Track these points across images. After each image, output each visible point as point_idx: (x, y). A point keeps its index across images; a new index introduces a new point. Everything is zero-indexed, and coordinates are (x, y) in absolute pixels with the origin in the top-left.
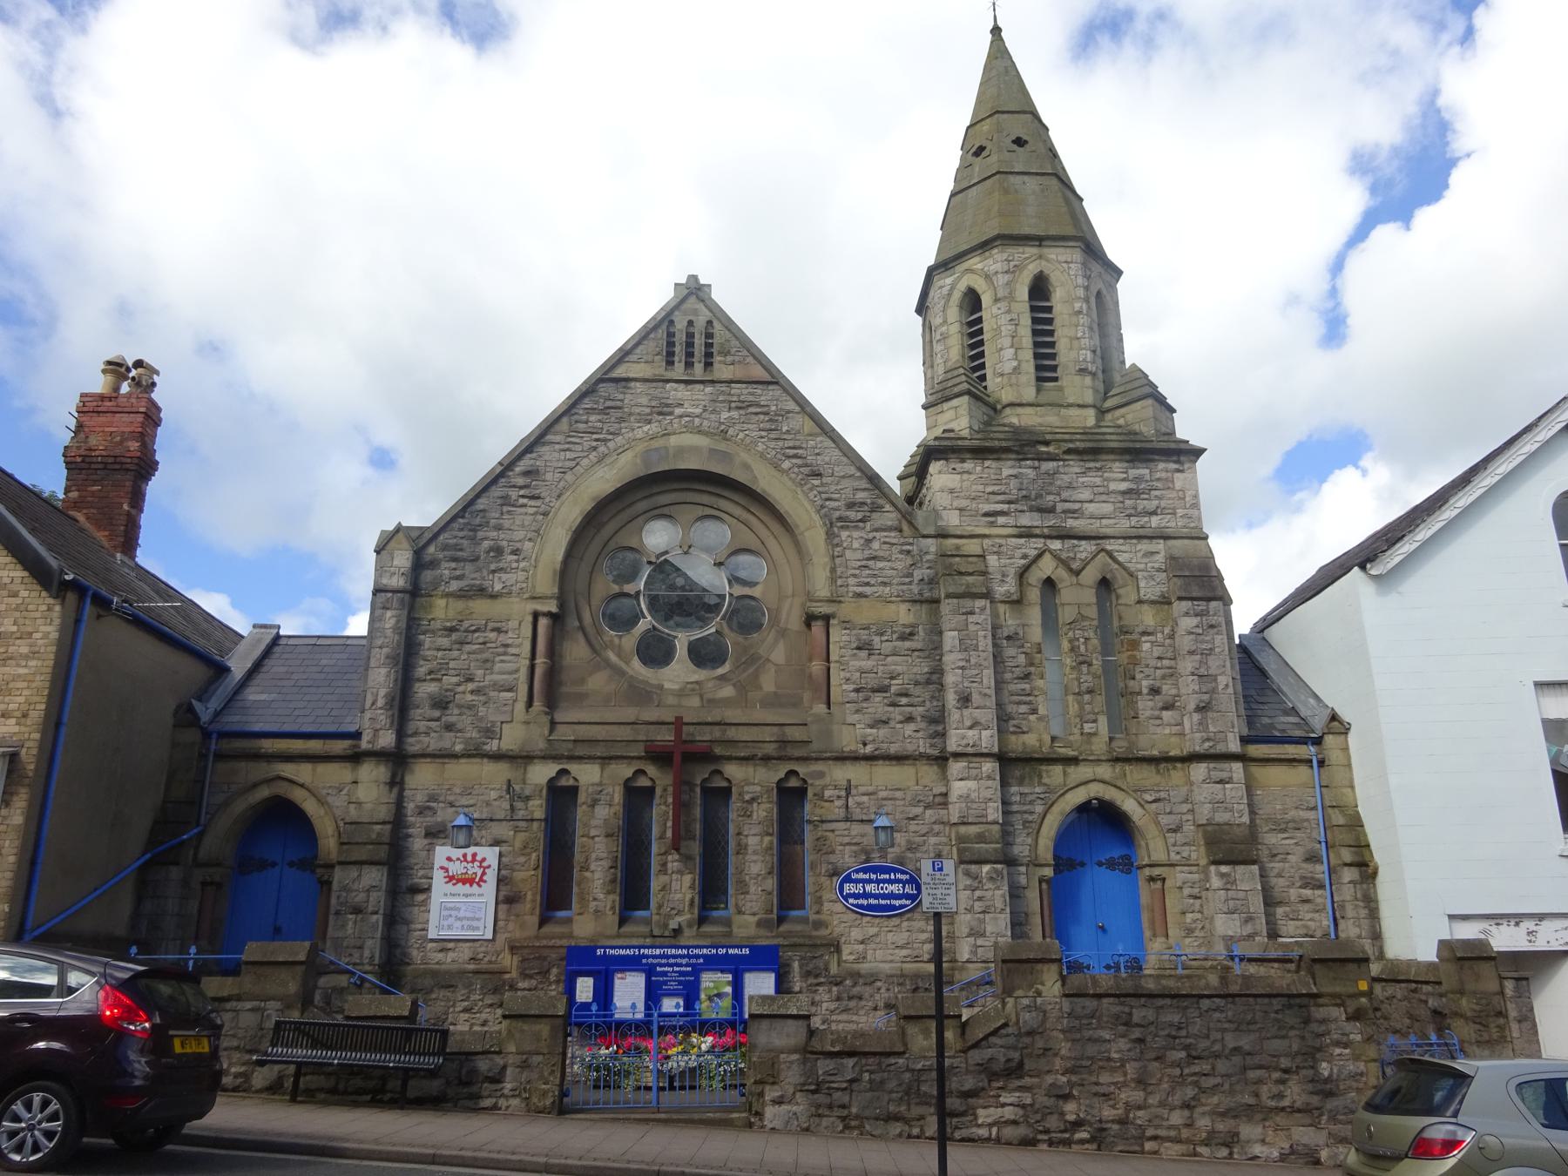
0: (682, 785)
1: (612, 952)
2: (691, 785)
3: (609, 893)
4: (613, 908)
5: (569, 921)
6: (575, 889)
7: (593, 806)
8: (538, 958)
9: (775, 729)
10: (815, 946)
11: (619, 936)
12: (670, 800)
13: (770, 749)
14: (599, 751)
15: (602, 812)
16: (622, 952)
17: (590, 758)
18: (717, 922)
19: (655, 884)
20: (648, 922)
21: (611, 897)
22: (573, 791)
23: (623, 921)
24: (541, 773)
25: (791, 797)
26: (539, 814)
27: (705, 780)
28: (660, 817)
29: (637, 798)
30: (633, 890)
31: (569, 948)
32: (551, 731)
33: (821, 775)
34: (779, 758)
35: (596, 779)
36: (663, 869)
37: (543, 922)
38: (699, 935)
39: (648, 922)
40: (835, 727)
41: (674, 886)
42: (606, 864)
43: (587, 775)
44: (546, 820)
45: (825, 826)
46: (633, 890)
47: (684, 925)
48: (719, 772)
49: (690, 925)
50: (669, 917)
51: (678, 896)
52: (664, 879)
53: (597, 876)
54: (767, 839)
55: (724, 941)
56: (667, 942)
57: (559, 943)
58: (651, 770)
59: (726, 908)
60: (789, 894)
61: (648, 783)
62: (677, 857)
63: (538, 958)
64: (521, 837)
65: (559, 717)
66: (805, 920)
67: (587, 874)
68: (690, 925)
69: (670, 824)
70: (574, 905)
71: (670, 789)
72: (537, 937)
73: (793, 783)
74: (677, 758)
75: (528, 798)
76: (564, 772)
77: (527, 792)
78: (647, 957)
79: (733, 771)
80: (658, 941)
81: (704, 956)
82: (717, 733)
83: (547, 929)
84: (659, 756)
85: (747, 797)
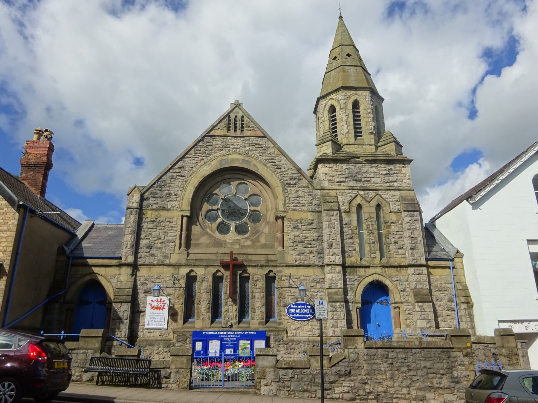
0: (233, 276)
3: (207, 312)
4: (209, 318)
6: (196, 311)
7: (202, 282)
10: (279, 331)
11: (211, 327)
12: (229, 280)
13: (263, 263)
14: (204, 263)
15: (205, 284)
16: (212, 333)
17: (201, 266)
18: (245, 323)
19: (223, 309)
20: (221, 323)
21: (208, 314)
22: (195, 277)
23: (212, 323)
24: (184, 271)
25: (270, 279)
26: (184, 285)
28: (225, 287)
29: (217, 280)
30: (215, 313)
31: (194, 332)
32: (188, 257)
35: (203, 273)
37: (184, 322)
38: (238, 327)
39: (221, 323)
41: (229, 310)
42: (207, 302)
43: (199, 272)
45: (282, 289)
46: (215, 313)
49: (235, 324)
51: (231, 314)
52: (226, 307)
53: (203, 306)
54: (262, 294)
55: (247, 329)
57: (190, 330)
58: (222, 270)
60: (269, 314)
64: (177, 293)
65: (190, 251)
67: (200, 306)
68: (235, 324)
69: (228, 288)
71: (229, 277)
72: (182, 328)
77: (179, 278)
78: (221, 335)
80: (224, 329)
81: (240, 334)
82: (245, 257)
85: (255, 279)
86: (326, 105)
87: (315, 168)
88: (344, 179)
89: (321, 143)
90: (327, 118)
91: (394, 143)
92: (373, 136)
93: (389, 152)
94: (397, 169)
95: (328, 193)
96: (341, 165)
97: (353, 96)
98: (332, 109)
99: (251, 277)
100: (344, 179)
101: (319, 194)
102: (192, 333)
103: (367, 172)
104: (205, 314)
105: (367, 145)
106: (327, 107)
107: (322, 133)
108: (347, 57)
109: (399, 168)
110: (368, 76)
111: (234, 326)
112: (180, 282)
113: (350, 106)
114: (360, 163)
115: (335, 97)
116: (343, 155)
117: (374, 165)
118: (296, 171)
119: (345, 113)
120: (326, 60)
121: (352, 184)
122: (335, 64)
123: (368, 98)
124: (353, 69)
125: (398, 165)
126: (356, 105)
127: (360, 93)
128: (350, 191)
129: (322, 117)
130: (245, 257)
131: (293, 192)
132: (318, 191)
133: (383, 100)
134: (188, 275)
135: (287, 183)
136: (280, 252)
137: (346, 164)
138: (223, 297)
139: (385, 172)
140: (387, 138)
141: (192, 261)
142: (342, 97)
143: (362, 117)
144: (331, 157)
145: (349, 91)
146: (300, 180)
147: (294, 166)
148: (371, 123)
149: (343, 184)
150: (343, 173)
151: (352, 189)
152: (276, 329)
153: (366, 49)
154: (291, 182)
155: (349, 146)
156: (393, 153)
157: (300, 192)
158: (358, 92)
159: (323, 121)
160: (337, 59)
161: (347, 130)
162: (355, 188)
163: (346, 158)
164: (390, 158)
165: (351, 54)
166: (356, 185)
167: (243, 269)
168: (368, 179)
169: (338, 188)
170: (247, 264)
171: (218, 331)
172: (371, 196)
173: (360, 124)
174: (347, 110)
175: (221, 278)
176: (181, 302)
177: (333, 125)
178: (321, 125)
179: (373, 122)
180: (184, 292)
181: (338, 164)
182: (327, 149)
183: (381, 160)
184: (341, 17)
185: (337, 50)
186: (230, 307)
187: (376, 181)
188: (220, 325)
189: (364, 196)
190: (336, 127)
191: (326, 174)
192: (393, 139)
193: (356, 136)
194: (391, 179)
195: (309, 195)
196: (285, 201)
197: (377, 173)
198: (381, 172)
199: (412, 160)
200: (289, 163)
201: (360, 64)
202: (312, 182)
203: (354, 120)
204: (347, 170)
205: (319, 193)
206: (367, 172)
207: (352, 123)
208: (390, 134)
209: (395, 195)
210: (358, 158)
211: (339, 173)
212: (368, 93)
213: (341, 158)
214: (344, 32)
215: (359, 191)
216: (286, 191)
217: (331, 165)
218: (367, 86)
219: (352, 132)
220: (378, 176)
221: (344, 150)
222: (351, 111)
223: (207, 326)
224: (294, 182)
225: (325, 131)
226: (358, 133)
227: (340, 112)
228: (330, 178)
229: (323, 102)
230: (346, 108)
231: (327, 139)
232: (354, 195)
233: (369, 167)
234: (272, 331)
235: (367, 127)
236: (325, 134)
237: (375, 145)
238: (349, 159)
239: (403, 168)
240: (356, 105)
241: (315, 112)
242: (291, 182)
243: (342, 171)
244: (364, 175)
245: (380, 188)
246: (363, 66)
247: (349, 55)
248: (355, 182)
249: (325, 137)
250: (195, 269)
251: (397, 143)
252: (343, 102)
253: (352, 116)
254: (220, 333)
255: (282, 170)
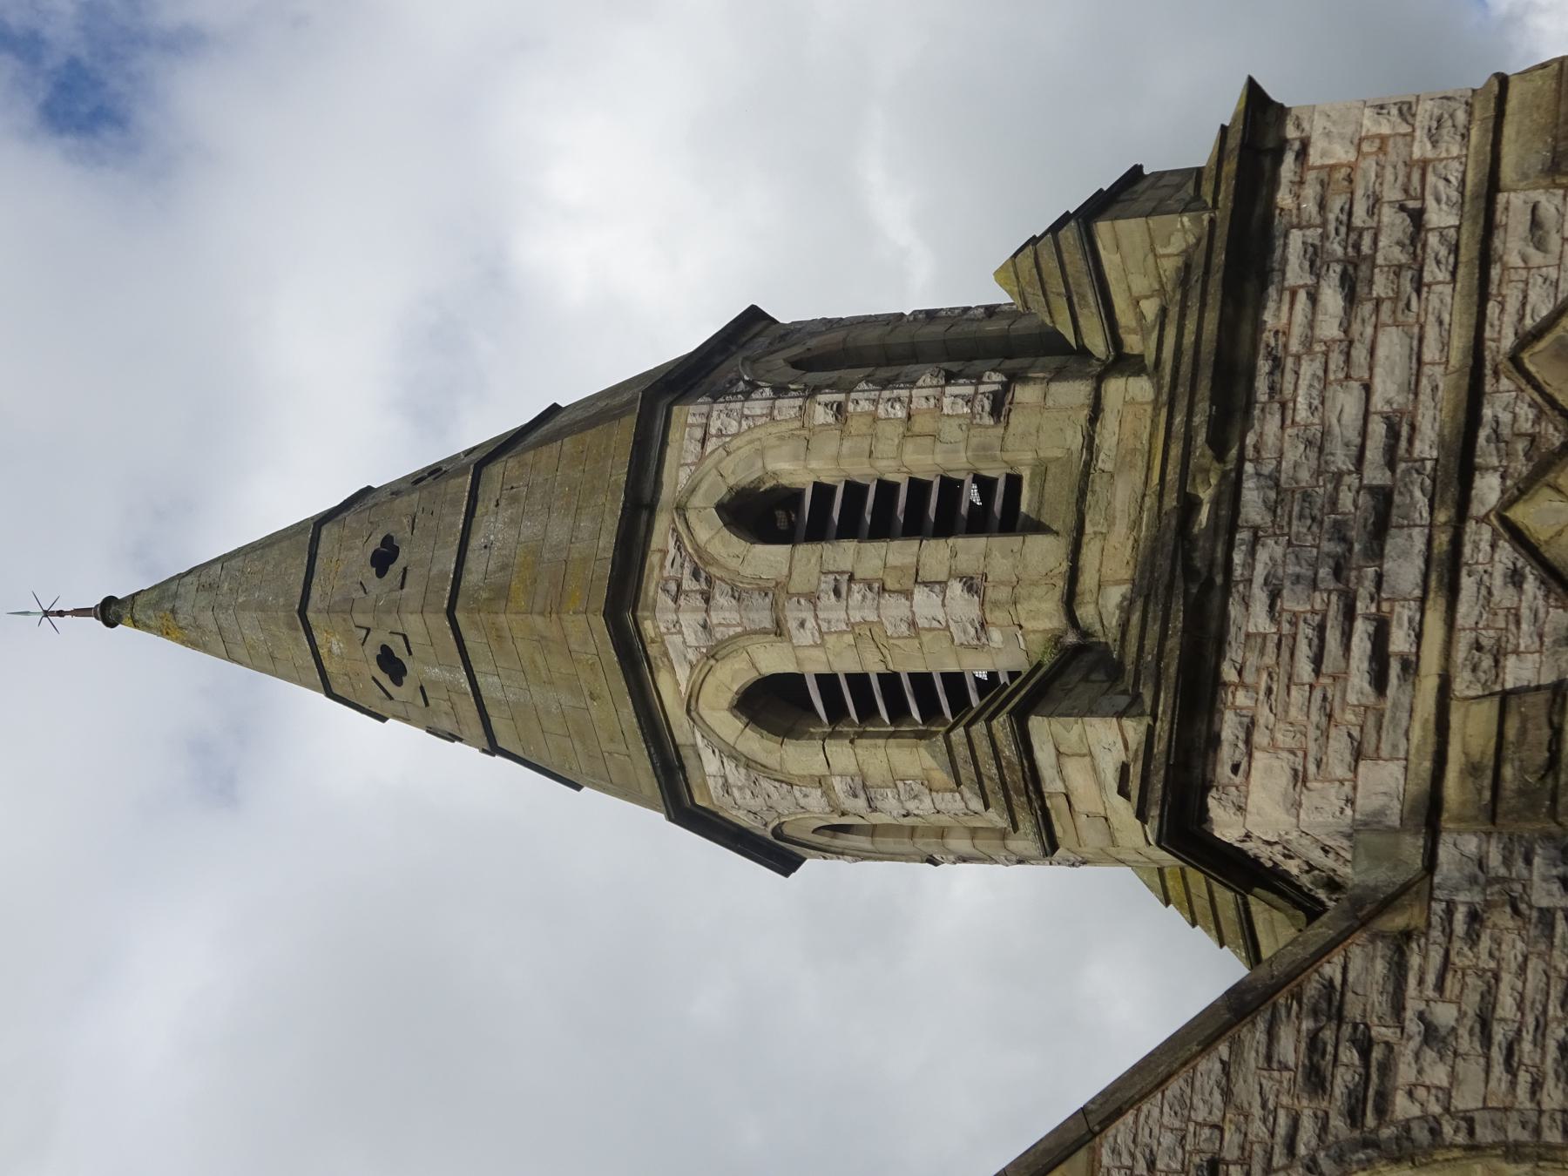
86: (734, 755)
87: (1240, 871)
88: (1362, 628)
89: (1030, 818)
90: (842, 755)
91: (1103, 228)
92: (1026, 394)
93: (1170, 266)
94: (1310, 206)
95: (1472, 770)
96: (1234, 653)
97: (691, 530)
98: (775, 703)
100: (1362, 628)
101: (1471, 844)
103: (1319, 444)
105: (1102, 437)
106: (755, 743)
107: (952, 803)
108: (395, 569)
109: (1310, 192)
110: (559, 421)
113: (769, 559)
114: (1231, 493)
115: (683, 674)
116: (1154, 629)
117: (1262, 385)
118: (1254, 1036)
119: (813, 598)
120: (401, 740)
121: (1405, 566)
122: (432, 667)
123: (724, 417)
124: (492, 527)
125: (1284, 198)
126: (761, 513)
127: (676, 476)
128: (1467, 583)
129: (827, 792)
131: (1438, 1074)
132: (1445, 853)
133: (753, 318)
135: (1354, 1115)
137: (1235, 610)
139: (1332, 299)
140: (1055, 284)
142: (690, 620)
143: (862, 471)
144: (1162, 728)
145: (654, 559)
146: (1332, 1005)
147: (1208, 1045)
148: (919, 403)
149: (1400, 641)
150: (1305, 631)
151: (1447, 571)
153: (324, 435)
154: (1343, 1080)
155: (1088, 580)
156: (1179, 233)
157: (1445, 1014)
158: (666, 494)
159: (863, 786)
160: (399, 652)
161: (956, 588)
162: (1443, 539)
163: (1178, 607)
164: (1220, 258)
165: (376, 542)
166: (1419, 543)
168: (1378, 428)
169: (1429, 684)
172: (1525, 413)
173: (918, 488)
174: (797, 585)
177: (898, 711)
178: (890, 809)
179: (912, 383)
181: (1229, 673)
182: (1090, 754)
183: (1228, 328)
184: (109, 612)
185: (333, 645)
187: (1401, 373)
189: (1521, 466)
190: (922, 681)
191: (1299, 778)
192: (1069, 234)
193: (1012, 522)
194: (1390, 250)
195: (1472, 938)
196: (1513, 1152)
197: (1336, 359)
198: (1329, 328)
199: (1252, 86)
200: (1175, 1087)
201: (461, 472)
202: (1357, 902)
203: (882, 530)
204: (1289, 603)
205: (1458, 848)
206: (1319, 444)
207: (900, 552)
208: (1026, 262)
209: (1536, 223)
210: (1189, 505)
211: (1305, 669)
212: (688, 418)
213: (1173, 643)
214: (211, 587)
215: (1477, 509)
216: (1421, 1134)
217: (1229, 728)
218: (630, 421)
219: (970, 550)
220: (1360, 354)
221: (1113, 621)
222: (804, 550)
224: (1349, 1055)
225: (941, 777)
226: (996, 510)
227: (805, 637)
228: (1339, 747)
229: (712, 776)
230: (776, 592)
231: (1009, 751)
232: (1506, 553)
233: (1272, 425)
235: (951, 431)
236: (967, 771)
237: (1100, 379)
238: (1189, 575)
239: (1314, 158)
240: (761, 513)
241: (779, 854)
242: (1343, 1080)
243: (1285, 645)
244: (1341, 460)
245: (1459, 342)
246: (475, 457)
247: (384, 558)
248: (1394, 542)
249: (989, 768)
251: (1101, 205)
252: (726, 614)
253: (849, 546)
255: (1231, 1153)
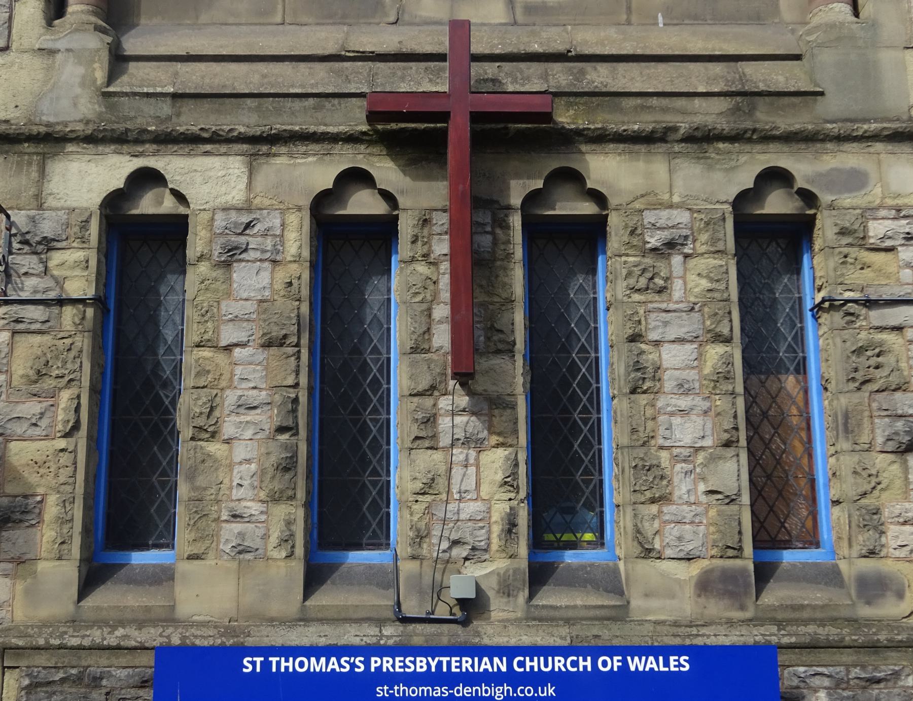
0: (477, 210)
1: (289, 665)
2: (498, 212)
3: (275, 498)
4: (287, 540)
5: (163, 577)
6: (183, 490)
7: (227, 265)
8: (78, 680)
9: (717, 68)
10: (874, 647)
11: (304, 619)
12: (441, 247)
13: (711, 114)
14: (245, 120)
15: (252, 281)
16: (317, 665)
17: (216, 138)
18: (580, 579)
19: (404, 474)
20: (388, 579)
21: (281, 511)
22: (174, 230)
23: (314, 578)
24: (87, 180)
25: (770, 241)
26: (81, 285)
27: (532, 198)
28: (414, 299)
29: (348, 246)
30: (341, 496)
31: (164, 654)
32: (112, 77)
33: (855, 180)
34: (735, 138)
35: (236, 193)
36: (426, 435)
37: (93, 577)
38: (535, 618)
39: (388, 579)
40: (886, 57)
41: (457, 481)
42: (267, 419)
43: (208, 183)
44: (99, 302)
45: (876, 316)
46: (341, 496)
47: (490, 588)
48: (572, 178)
49: (506, 589)
50: (446, 564)
51: (470, 508)
52: (428, 460)
53: (240, 451)
54: (715, 352)
55: (609, 634)
56: (446, 635)
57: (137, 636)
58: (386, 171)
59: (600, 542)
60: (777, 505)
61: (378, 207)
62: (463, 401)
63: (78, 680)
64: (30, 348)
65: (132, 44)
66: (830, 576)
67: (214, 448)
68: (506, 589)
69: (442, 311)
70: (183, 535)
71: (442, 220)
72: (73, 622)
73: (777, 203)
74: (459, 131)
75: (49, 244)
76: (146, 179)
77: (47, 228)
78: (391, 679)
79: (605, 168)
80: (420, 634)
81: (554, 677)
82: (560, 77)
83: (105, 598)
84: (411, 133)
85: (654, 240)
99: (614, 221)
102: (148, 659)
104: (254, 508)
111: (499, 608)
112: (56, 258)
130: (560, 77)
134: (114, 203)
136: (836, 36)
138: (401, 378)
141: (150, 108)
152: (848, 635)
167: (554, 163)
170: (582, 124)
171: (367, 651)
175: (380, 234)
176: (62, 415)
180: (83, 342)
186: (459, 454)
188: (382, 601)
215: (699, 628)
223: (275, 608)
234: (813, 646)
250: (174, 166)
254: (387, 664)
